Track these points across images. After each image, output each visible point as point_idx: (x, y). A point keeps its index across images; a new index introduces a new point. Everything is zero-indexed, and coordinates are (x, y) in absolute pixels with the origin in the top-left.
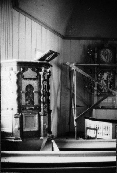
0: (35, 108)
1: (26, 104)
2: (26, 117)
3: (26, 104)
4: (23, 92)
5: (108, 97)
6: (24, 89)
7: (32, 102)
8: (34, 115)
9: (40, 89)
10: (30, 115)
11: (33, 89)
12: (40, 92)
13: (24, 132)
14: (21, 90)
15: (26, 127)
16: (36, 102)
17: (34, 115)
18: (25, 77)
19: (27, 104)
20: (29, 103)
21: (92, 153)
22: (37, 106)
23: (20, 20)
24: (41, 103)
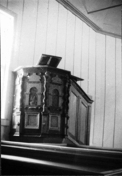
0: (37, 108)
1: (29, 104)
2: (29, 116)
3: (29, 104)
4: (27, 94)
5: (69, 99)
6: (28, 91)
7: (35, 103)
8: (36, 115)
9: (46, 91)
10: (32, 115)
11: (37, 91)
12: (43, 94)
13: (26, 129)
14: (26, 91)
15: (28, 125)
16: (39, 103)
17: (36, 115)
18: (30, 81)
19: (31, 104)
20: (33, 103)
21: (65, 148)
22: (39, 106)
23: (116, 103)
24: (45, 103)
